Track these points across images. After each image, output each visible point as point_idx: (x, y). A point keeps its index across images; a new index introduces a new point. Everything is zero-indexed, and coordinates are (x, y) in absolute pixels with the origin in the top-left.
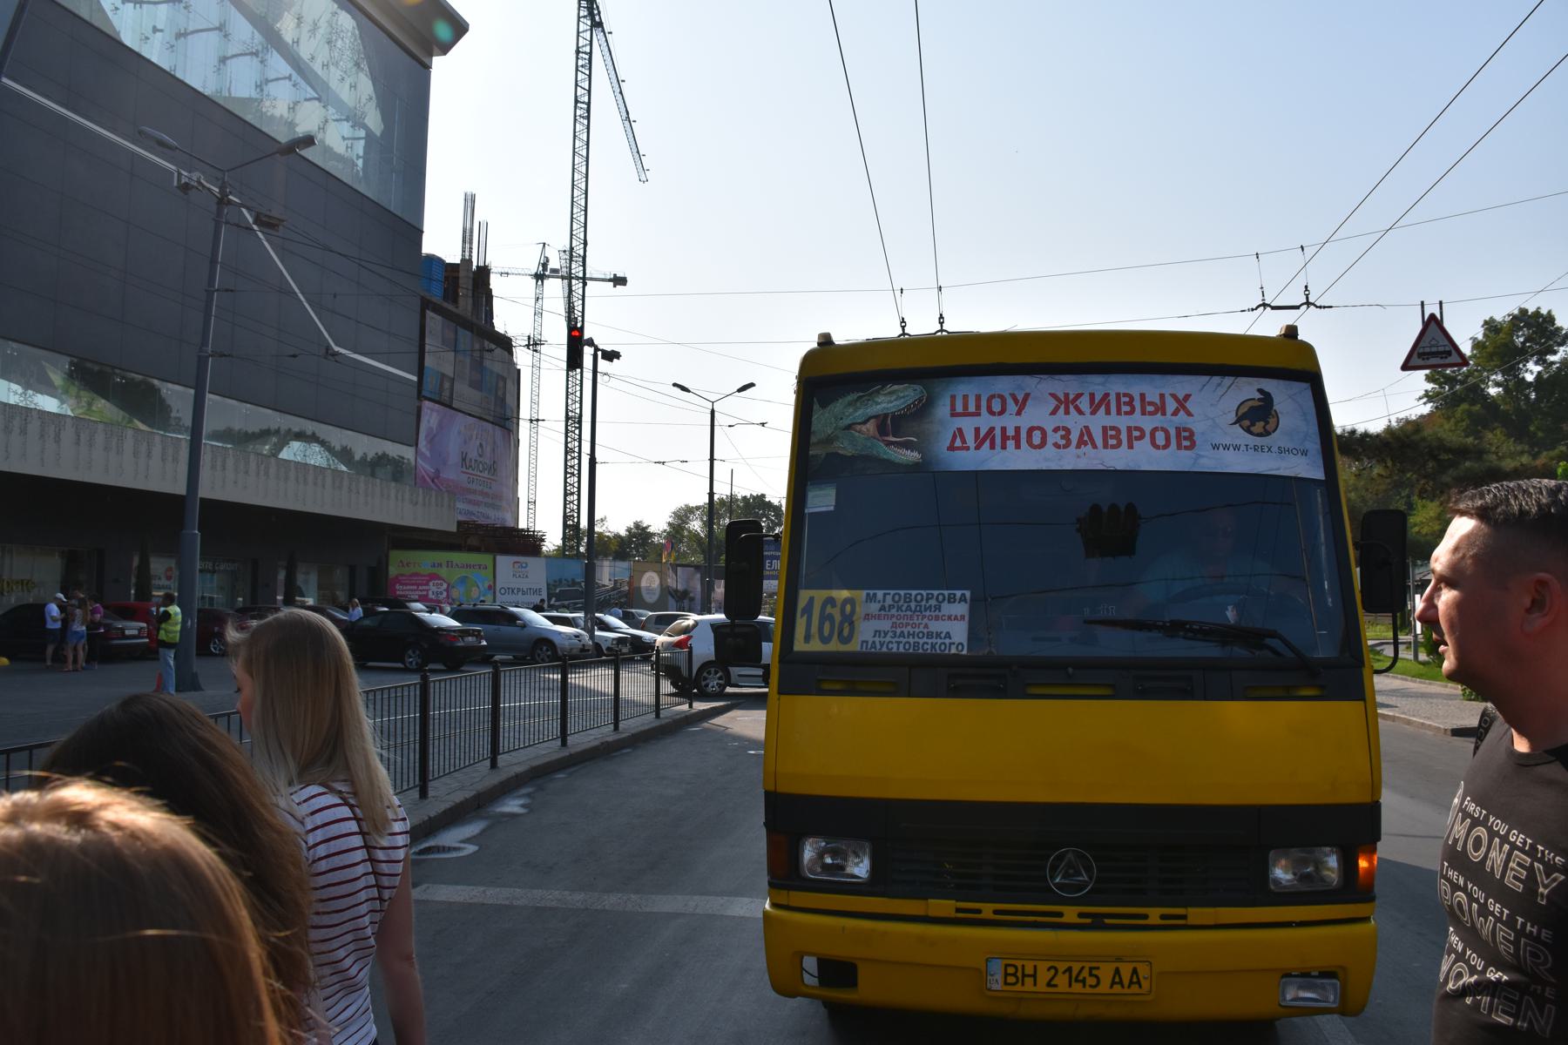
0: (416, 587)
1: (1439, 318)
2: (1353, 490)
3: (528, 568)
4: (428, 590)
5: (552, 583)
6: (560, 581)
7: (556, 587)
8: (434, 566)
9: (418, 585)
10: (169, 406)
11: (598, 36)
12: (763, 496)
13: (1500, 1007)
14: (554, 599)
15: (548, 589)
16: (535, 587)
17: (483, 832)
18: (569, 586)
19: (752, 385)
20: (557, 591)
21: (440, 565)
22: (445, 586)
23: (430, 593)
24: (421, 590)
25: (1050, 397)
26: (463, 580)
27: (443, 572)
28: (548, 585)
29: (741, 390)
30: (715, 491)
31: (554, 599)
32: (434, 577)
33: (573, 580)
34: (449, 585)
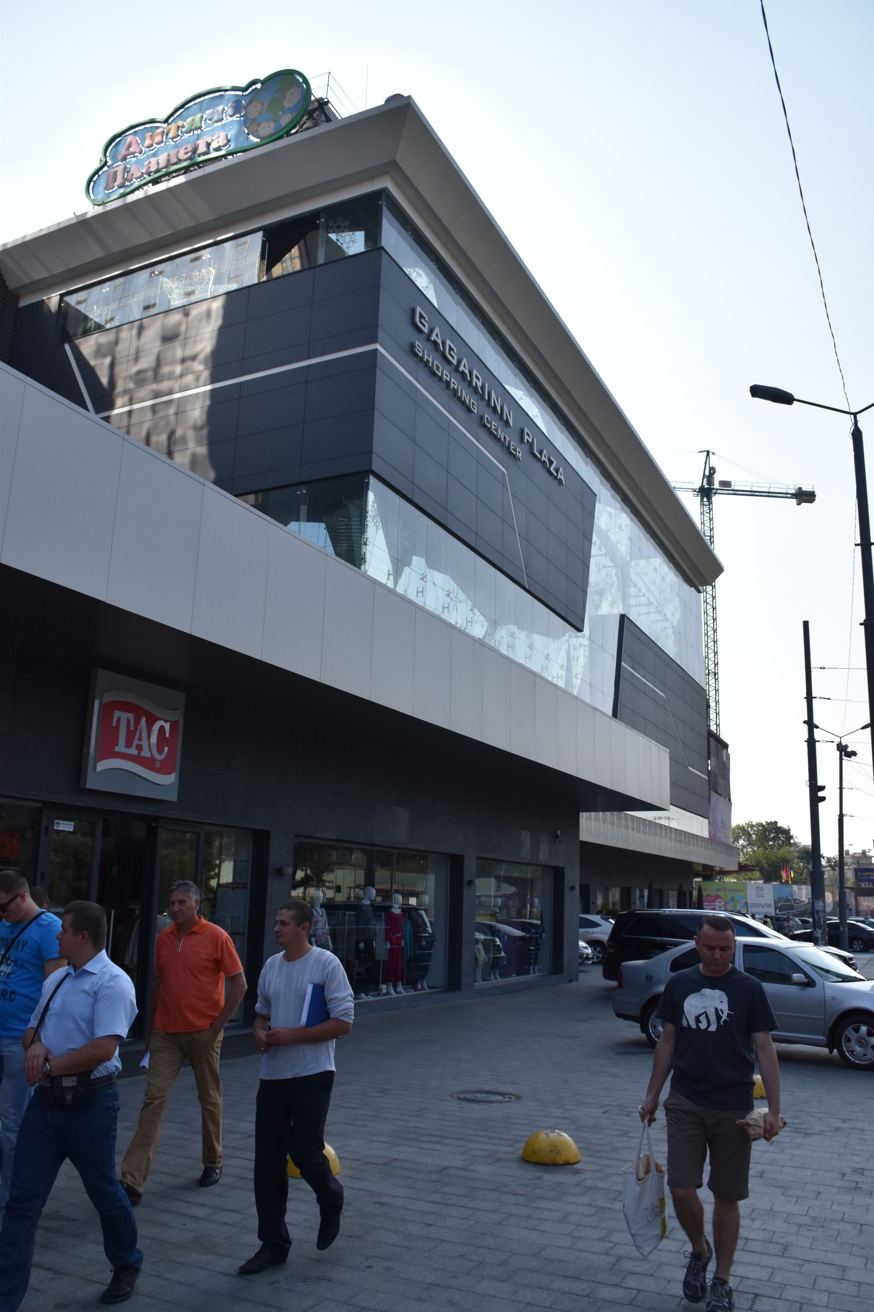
0: (709, 904)
1: (104, 380)
2: (213, 876)
3: (764, 891)
4: (715, 905)
5: (776, 900)
6: (780, 898)
7: (778, 902)
8: (717, 890)
9: (710, 902)
10: (389, 100)
11: (866, 1173)
12: (776, 823)
13: (480, 984)
14: (778, 910)
15: (775, 904)
16: (768, 903)
17: (225, 973)
18: (785, 902)
19: (758, 391)
20: (779, 905)
21: (720, 890)
22: (723, 903)
23: (716, 907)
24: (712, 905)
25: (126, 720)
26: (733, 899)
27: (722, 894)
28: (775, 901)
29: (782, 397)
30: (844, 812)
31: (778, 910)
32: (718, 897)
33: (787, 898)
34: (725, 901)
